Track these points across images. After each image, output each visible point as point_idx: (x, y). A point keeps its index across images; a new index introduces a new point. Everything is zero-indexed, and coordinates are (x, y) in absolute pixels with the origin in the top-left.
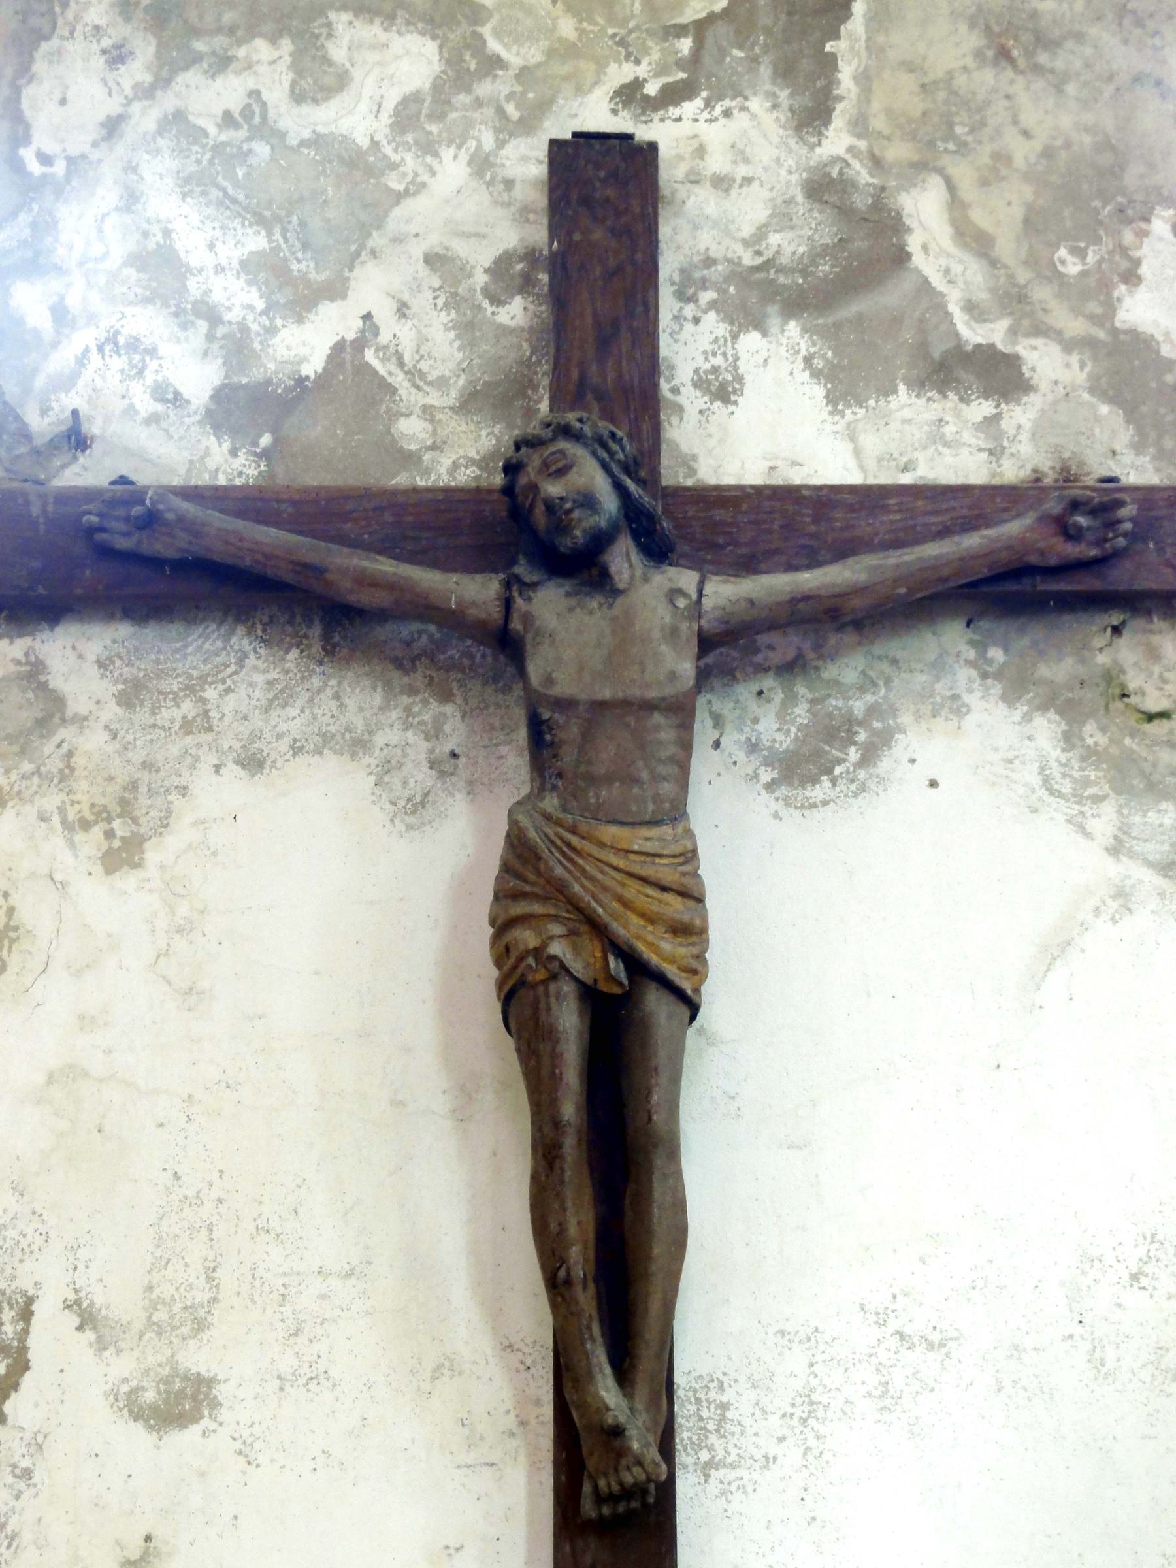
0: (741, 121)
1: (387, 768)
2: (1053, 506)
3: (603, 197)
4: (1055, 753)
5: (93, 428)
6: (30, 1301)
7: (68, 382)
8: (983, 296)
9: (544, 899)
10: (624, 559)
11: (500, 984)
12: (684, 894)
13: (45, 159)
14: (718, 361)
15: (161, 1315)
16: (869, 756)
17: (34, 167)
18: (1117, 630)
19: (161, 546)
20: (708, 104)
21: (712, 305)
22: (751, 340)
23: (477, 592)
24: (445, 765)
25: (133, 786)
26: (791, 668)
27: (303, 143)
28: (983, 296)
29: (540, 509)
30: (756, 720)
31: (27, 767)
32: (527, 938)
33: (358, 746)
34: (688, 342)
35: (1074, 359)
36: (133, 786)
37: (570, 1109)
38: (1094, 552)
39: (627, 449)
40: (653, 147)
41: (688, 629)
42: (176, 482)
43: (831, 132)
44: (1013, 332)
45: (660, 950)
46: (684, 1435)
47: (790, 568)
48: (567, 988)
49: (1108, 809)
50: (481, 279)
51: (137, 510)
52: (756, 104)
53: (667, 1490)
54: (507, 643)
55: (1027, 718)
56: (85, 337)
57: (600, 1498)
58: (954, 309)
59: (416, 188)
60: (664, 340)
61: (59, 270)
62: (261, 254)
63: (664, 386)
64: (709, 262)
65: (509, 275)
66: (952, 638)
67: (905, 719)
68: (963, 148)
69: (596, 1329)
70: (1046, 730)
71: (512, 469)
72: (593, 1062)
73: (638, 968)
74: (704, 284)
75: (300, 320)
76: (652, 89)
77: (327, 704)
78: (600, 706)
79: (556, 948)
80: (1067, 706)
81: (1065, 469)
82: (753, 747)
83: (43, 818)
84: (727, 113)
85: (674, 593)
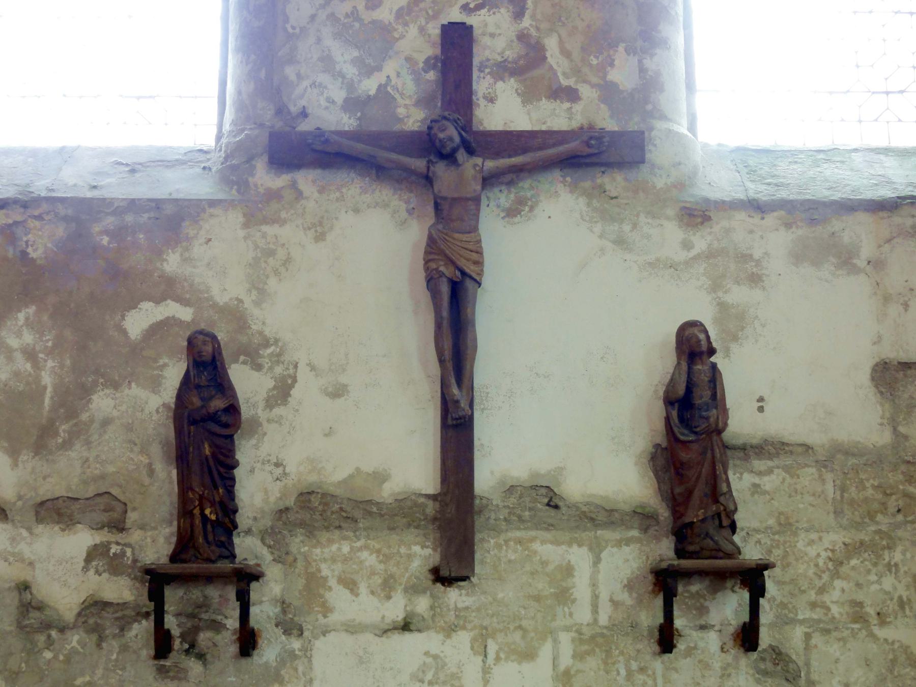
0: (498, 15)
1: (395, 212)
2: (585, 138)
3: (457, 42)
4: (585, 208)
5: (309, 111)
6: (297, 363)
7: (301, 97)
8: (568, 71)
9: (439, 254)
10: (461, 155)
11: (426, 277)
12: (477, 252)
13: (293, 28)
14: (490, 90)
15: (333, 367)
16: (532, 209)
17: (290, 30)
18: (603, 172)
19: (329, 149)
20: (489, 11)
21: (489, 73)
22: (500, 84)
23: (419, 164)
24: (410, 212)
25: (322, 217)
26: (510, 183)
27: (370, 23)
28: (568, 71)
29: (437, 141)
30: (501, 197)
31: (293, 212)
32: (433, 265)
33: (386, 206)
34: (481, 85)
35: (594, 90)
36: (322, 217)
37: (445, 313)
38: (596, 151)
39: (462, 121)
40: (471, 27)
41: (479, 177)
42: (333, 129)
43: (525, 19)
44: (576, 82)
45: (470, 269)
46: (477, 401)
47: (510, 156)
48: (445, 280)
49: (599, 225)
50: (421, 65)
51: (323, 139)
52: (503, 10)
53: (471, 418)
54: (428, 179)
55: (577, 198)
56: (306, 83)
57: (453, 419)
58: (559, 74)
59: (402, 37)
60: (474, 84)
61: (299, 62)
62: (357, 57)
63: (474, 98)
64: (488, 60)
65: (430, 64)
66: (557, 174)
67: (542, 198)
68: (564, 24)
69: (452, 373)
70: (582, 201)
71: (430, 128)
72: (453, 295)
73: (463, 273)
74: (486, 67)
75: (369, 78)
76: (472, 6)
77: (377, 193)
78: (454, 200)
79: (442, 269)
80: (589, 196)
81: (590, 124)
82: (498, 206)
83: (297, 226)
84: (494, 13)
85: (476, 165)
